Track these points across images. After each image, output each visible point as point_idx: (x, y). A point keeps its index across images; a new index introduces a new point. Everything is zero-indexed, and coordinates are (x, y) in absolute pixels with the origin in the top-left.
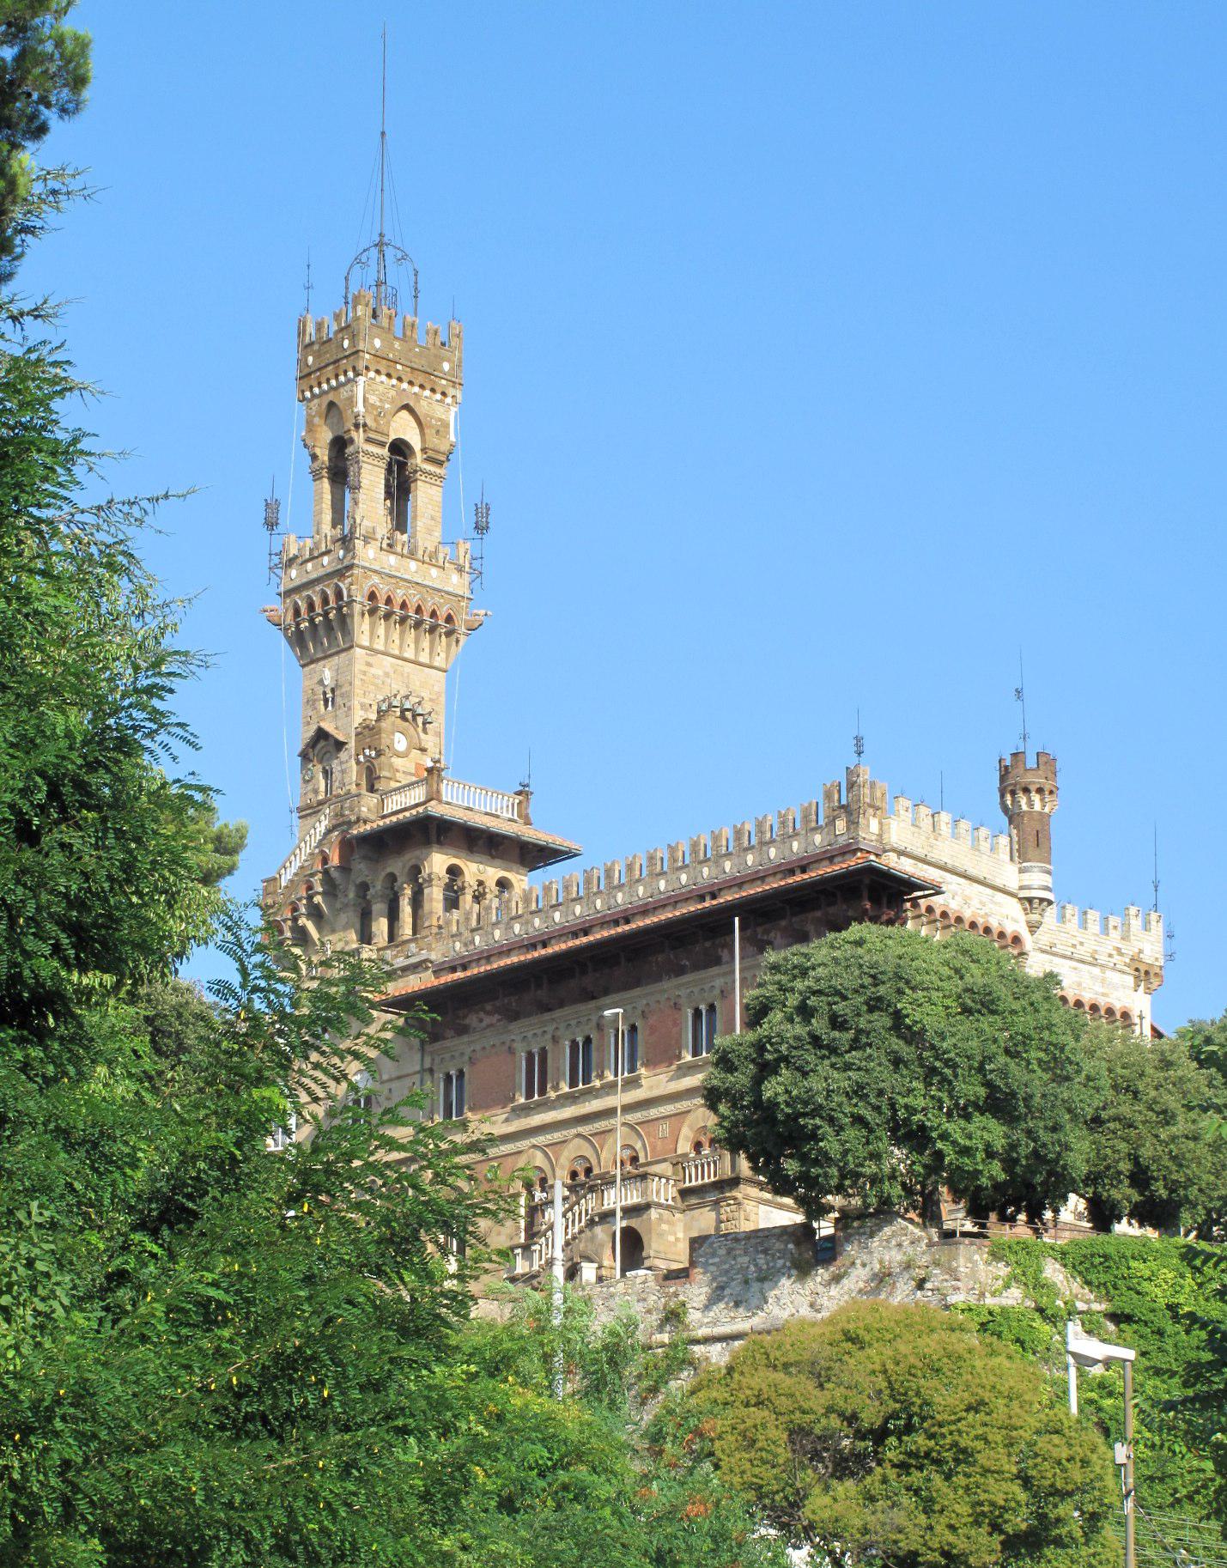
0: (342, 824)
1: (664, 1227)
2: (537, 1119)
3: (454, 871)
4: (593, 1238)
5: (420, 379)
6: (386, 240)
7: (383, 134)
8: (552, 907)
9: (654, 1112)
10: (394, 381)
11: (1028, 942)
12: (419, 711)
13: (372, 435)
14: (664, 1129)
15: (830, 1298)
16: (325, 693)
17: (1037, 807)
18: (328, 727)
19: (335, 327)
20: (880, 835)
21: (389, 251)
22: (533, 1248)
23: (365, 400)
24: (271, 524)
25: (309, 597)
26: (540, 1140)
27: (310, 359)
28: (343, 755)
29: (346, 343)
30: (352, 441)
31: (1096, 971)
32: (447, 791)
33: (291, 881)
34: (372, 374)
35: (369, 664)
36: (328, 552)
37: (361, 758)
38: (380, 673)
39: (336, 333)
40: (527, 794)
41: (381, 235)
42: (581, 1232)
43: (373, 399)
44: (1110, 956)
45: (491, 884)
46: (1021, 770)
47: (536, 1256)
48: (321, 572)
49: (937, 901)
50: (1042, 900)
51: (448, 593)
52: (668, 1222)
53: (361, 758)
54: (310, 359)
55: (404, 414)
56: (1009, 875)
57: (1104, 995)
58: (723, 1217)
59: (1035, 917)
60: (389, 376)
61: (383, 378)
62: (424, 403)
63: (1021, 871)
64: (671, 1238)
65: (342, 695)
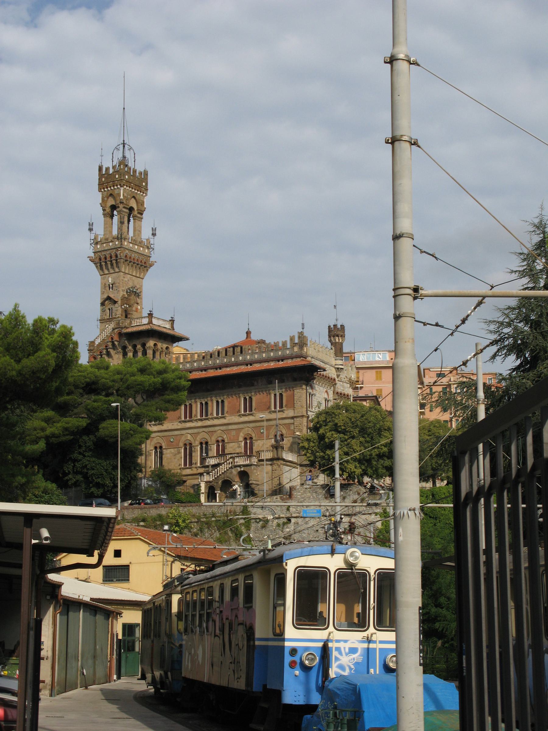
0: (118, 326)
1: (255, 471)
2: (189, 425)
3: (155, 345)
4: (231, 473)
5: (137, 188)
6: (125, 142)
7: (124, 108)
8: (193, 361)
9: (230, 427)
10: (131, 189)
11: (337, 379)
12: (137, 292)
14: (234, 433)
16: (109, 285)
17: (337, 341)
18: (112, 296)
20: (306, 352)
21: (126, 146)
22: (210, 474)
23: (123, 195)
24: (91, 230)
26: (190, 431)
27: (103, 179)
28: (116, 305)
29: (117, 176)
30: (119, 207)
31: (341, 383)
32: (155, 321)
33: (99, 343)
34: (125, 187)
36: (112, 241)
37: (123, 307)
38: (127, 280)
39: (113, 172)
40: (174, 321)
41: (124, 141)
43: (125, 195)
44: (345, 378)
45: (164, 348)
47: (211, 476)
48: (109, 248)
49: (325, 373)
50: (341, 368)
51: (145, 255)
52: (256, 470)
54: (103, 179)
55: (133, 199)
56: (333, 362)
57: (343, 390)
58: (273, 469)
59: (339, 373)
60: (129, 187)
61: (128, 188)
62: (138, 196)
64: (257, 474)
65: (116, 286)
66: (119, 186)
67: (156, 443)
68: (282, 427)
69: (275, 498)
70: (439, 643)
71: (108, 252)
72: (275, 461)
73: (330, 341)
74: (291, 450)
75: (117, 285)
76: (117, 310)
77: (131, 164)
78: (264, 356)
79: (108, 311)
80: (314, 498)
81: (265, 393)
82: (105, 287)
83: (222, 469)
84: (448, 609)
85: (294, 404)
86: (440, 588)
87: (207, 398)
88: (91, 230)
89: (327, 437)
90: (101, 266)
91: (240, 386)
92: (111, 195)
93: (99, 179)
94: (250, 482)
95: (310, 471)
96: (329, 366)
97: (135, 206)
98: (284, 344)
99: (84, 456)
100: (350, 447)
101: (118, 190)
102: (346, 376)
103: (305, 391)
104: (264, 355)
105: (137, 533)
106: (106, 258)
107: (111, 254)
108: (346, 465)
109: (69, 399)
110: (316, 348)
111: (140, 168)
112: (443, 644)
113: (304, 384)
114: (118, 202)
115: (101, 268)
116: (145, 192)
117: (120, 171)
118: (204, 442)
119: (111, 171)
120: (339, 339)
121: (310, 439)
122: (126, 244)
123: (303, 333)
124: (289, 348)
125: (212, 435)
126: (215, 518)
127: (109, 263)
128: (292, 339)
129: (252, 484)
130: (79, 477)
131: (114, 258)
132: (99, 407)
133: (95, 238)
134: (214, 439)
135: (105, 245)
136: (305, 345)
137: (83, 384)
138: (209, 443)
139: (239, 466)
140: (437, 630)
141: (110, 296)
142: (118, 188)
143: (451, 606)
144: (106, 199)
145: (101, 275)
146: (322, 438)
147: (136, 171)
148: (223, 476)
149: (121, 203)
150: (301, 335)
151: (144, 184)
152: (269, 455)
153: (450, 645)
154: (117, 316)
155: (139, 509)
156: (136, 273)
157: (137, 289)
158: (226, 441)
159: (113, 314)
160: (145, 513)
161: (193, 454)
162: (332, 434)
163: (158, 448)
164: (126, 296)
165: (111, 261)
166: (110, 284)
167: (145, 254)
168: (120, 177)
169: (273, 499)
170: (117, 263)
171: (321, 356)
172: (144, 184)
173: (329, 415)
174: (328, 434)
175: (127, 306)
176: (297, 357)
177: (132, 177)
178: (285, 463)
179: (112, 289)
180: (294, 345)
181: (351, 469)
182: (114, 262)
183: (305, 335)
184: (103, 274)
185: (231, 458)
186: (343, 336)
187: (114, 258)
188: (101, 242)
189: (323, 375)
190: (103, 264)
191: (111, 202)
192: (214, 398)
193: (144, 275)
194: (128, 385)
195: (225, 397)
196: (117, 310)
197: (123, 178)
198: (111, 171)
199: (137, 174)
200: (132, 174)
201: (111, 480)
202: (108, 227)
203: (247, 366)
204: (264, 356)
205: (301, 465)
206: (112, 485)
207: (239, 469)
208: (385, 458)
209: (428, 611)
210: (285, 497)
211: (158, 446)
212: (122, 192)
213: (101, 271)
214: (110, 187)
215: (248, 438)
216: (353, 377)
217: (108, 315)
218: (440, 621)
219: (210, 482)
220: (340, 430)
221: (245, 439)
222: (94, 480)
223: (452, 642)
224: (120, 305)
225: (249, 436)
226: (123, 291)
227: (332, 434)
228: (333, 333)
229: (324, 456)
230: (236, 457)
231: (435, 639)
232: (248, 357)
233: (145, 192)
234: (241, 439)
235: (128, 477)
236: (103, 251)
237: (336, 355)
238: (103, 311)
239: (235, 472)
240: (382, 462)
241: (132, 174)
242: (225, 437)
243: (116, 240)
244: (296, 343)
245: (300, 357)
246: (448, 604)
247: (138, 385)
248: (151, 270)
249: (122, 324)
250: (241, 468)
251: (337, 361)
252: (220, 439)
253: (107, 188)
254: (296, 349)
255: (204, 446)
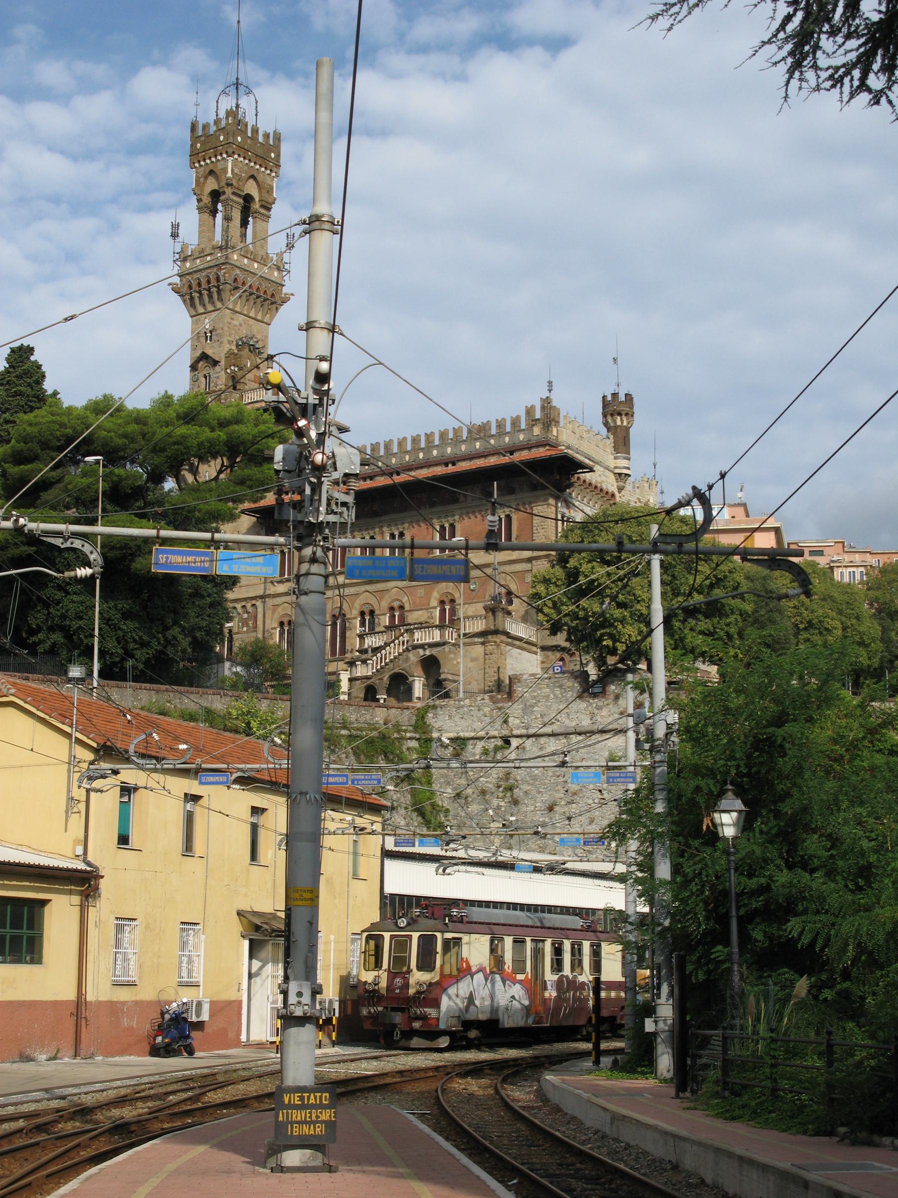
1: (452, 656)
4: (407, 659)
5: (260, 161)
6: (240, 81)
10: (247, 161)
12: (257, 346)
13: (236, 191)
15: (602, 717)
16: (206, 333)
17: (619, 423)
18: (209, 352)
19: (215, 128)
21: (241, 88)
23: (232, 171)
24: (175, 235)
25: (199, 279)
27: (199, 145)
28: (217, 368)
29: (222, 138)
30: (224, 193)
34: (236, 156)
35: (232, 319)
39: (215, 131)
41: (237, 79)
42: (400, 654)
43: (236, 170)
46: (617, 403)
47: (370, 666)
48: (206, 265)
50: (626, 475)
53: (229, 371)
54: (199, 145)
55: (251, 181)
56: (611, 462)
58: (487, 652)
59: (621, 484)
61: (242, 159)
63: (615, 458)
64: (455, 662)
65: (217, 335)
66: (225, 156)
67: (282, 616)
68: (509, 577)
69: (479, 698)
70: (802, 986)
71: (204, 274)
72: (490, 637)
73: (606, 424)
74: (525, 619)
75: (219, 331)
76: (218, 378)
77: (250, 120)
78: (477, 447)
79: (203, 380)
80: (556, 697)
81: (479, 516)
82: (199, 337)
83: (392, 651)
84: (831, 874)
85: (533, 533)
86: (805, 809)
87: (373, 528)
88: (175, 235)
89: (583, 572)
90: (192, 299)
91: (433, 505)
92: (212, 172)
93: (192, 145)
94: (443, 676)
95: (562, 659)
96: (602, 469)
97: (255, 194)
98: (515, 422)
99: (67, 593)
100: (629, 593)
101: (222, 162)
102: (639, 499)
103: (554, 508)
104: (478, 445)
105: (9, 689)
106: (199, 285)
107: (208, 277)
108: (620, 627)
109: (28, 471)
110: (577, 430)
111: (266, 126)
112: (815, 990)
113: (552, 496)
114: (223, 183)
115: (193, 305)
116: (275, 169)
117: (228, 128)
118: (367, 611)
119: (213, 129)
120: (621, 419)
121: (549, 580)
122: (235, 257)
123: (551, 400)
124: (524, 430)
125: (381, 598)
126: (349, 730)
127: (205, 292)
128: (529, 411)
129: (445, 680)
130: (57, 637)
131: (213, 283)
132: (89, 487)
133: (182, 251)
134: (385, 604)
135: (198, 261)
136: (553, 423)
137: (59, 440)
138: (377, 612)
139: (422, 646)
140: (793, 942)
141: (206, 351)
142: (223, 159)
143: (840, 863)
144: (202, 180)
145: (192, 317)
146: (573, 576)
147: (257, 131)
148: (391, 665)
149: (229, 185)
150: (546, 404)
151: (273, 155)
152: (479, 626)
153: (839, 994)
154: (218, 388)
155: (153, 692)
156: (257, 313)
157: (257, 342)
158: (407, 607)
159: (212, 385)
160: (169, 702)
161: (348, 634)
162: (593, 568)
163: (286, 624)
164: (236, 351)
165: (209, 290)
166: (208, 331)
167: (273, 279)
168: (226, 138)
169: (476, 701)
170: (219, 292)
171: (584, 447)
172: (273, 155)
173: (587, 531)
174: (585, 568)
175: (236, 369)
176: (538, 445)
177: (249, 141)
178: (510, 640)
179: (211, 340)
180: (533, 422)
181: (630, 635)
182: (214, 290)
183: (554, 404)
184: (195, 313)
185: (407, 631)
186: (630, 415)
187: (213, 283)
188: (192, 257)
189: (584, 481)
190: (196, 295)
191: (211, 185)
192: (385, 529)
193: (272, 318)
194: (156, 444)
195: (406, 525)
196: (218, 378)
197: (231, 140)
198: (213, 129)
199: (261, 139)
200: (249, 134)
201: (119, 643)
202: (205, 230)
203: (447, 466)
204: (477, 447)
205: (544, 648)
206: (120, 651)
207: (421, 652)
208: (700, 616)
209: (763, 881)
210: (499, 697)
211: (286, 620)
212: (230, 166)
213: (191, 309)
214: (210, 158)
215: (447, 600)
216: (651, 501)
217: (203, 386)
218: (805, 912)
219: (367, 678)
220: (609, 558)
221: (442, 602)
222: (82, 641)
223: (846, 985)
224: (223, 367)
225: (450, 597)
226: (230, 342)
227: (593, 568)
228: (610, 409)
229: (575, 612)
230: (417, 629)
231: (787, 973)
232: (449, 450)
233: (275, 169)
234: (434, 602)
235: (158, 639)
236: (196, 272)
237: (616, 449)
238: (194, 380)
239: (414, 657)
240: (693, 622)
241: (249, 134)
242: (405, 599)
243: (217, 251)
244: (538, 419)
245: (544, 445)
246: (832, 856)
247: (175, 443)
248: (284, 309)
249: (226, 400)
250: (425, 649)
251: (618, 461)
252: (396, 604)
253: (204, 160)
254: (537, 430)
255: (367, 618)
